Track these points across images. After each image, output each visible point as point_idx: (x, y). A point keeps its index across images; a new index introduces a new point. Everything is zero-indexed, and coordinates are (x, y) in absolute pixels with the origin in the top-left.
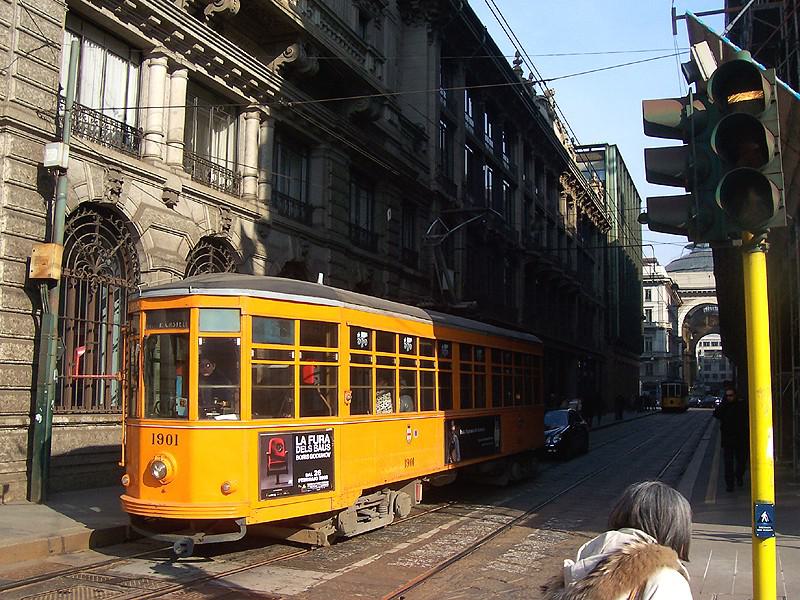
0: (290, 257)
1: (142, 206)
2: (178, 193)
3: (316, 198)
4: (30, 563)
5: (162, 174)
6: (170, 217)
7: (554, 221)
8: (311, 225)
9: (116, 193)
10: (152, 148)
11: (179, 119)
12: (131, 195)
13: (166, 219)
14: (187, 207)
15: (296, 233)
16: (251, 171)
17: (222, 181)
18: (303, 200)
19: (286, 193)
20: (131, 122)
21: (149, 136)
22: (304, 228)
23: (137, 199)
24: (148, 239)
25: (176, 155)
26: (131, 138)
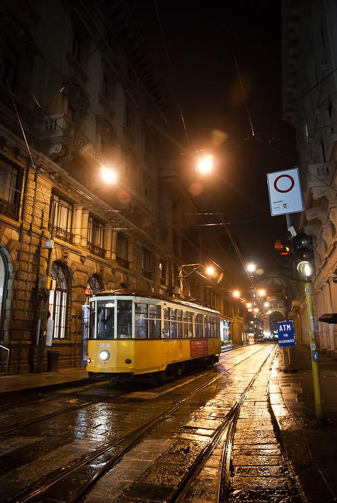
0: (122, 281)
1: (73, 263)
2: (85, 257)
3: (130, 259)
4: (321, 257)
5: (80, 250)
6: (83, 266)
7: (224, 275)
8: (128, 269)
9: (66, 257)
10: (77, 240)
11: (85, 232)
12: (7, 240)
13: (81, 267)
14: (88, 262)
15: (98, 261)
16: (109, 249)
17: (98, 252)
18: (101, 247)
19: (126, 260)
20: (69, 230)
21: (76, 236)
22: (101, 259)
23: (73, 258)
24: (75, 275)
25: (84, 243)
26: (70, 238)
